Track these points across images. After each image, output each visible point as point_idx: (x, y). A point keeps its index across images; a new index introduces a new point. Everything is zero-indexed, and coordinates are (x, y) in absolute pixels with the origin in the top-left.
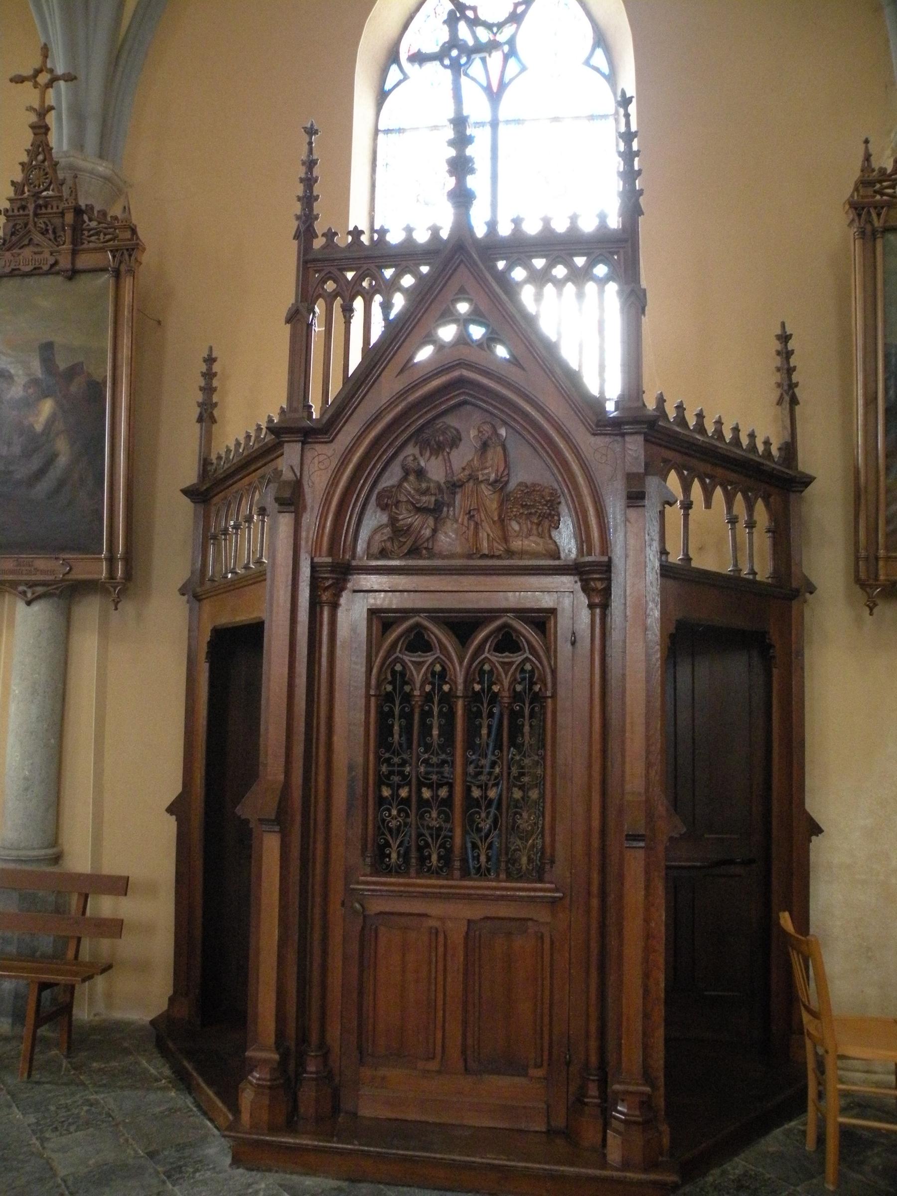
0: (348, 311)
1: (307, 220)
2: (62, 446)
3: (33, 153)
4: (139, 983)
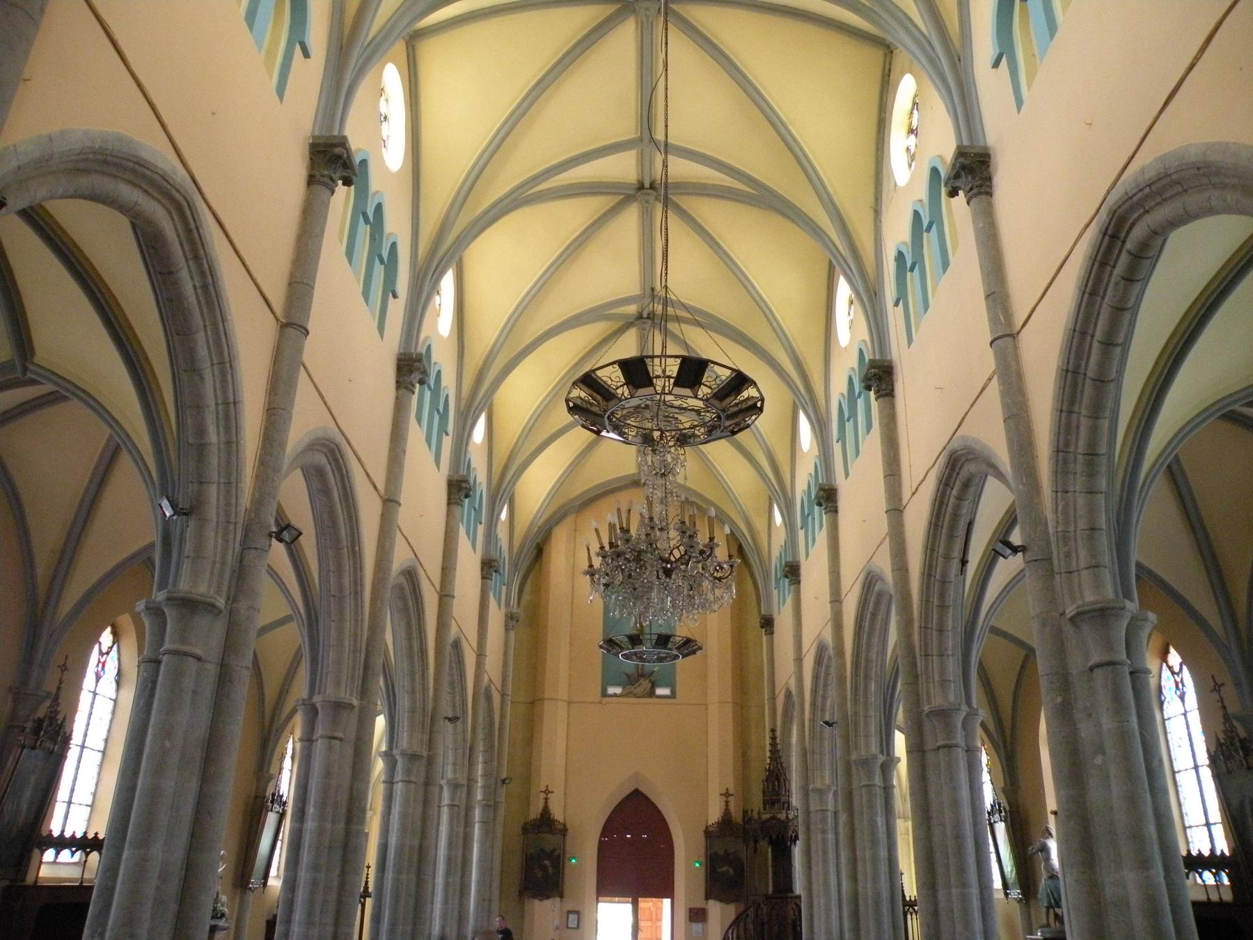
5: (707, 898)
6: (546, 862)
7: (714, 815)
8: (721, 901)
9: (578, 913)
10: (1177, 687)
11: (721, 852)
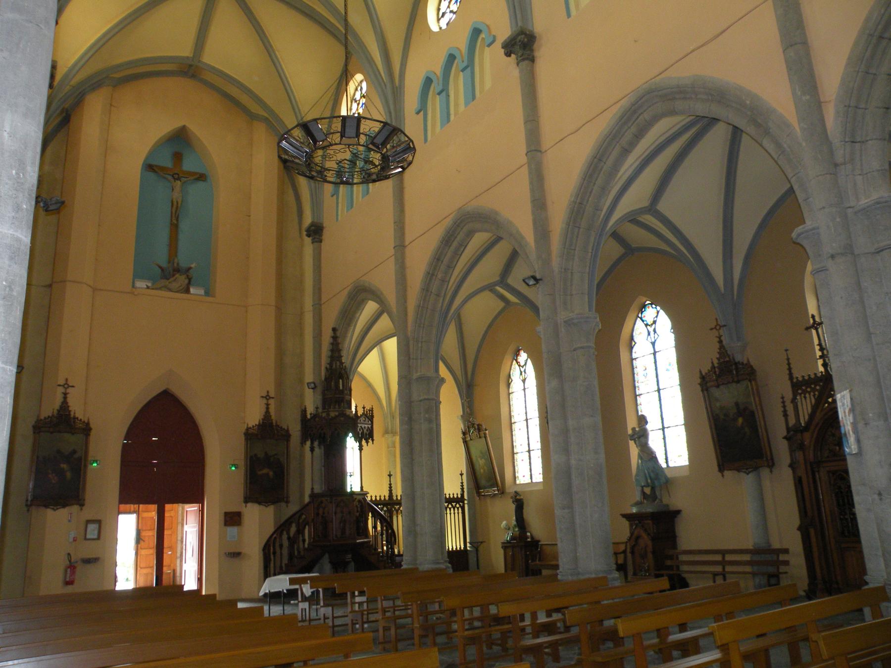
0: (805, 397)
1: (791, 375)
2: (747, 430)
3: (720, 349)
4: (797, 567)
5: (247, 500)
6: (64, 466)
7: (254, 417)
8: (259, 503)
9: (99, 522)
10: (521, 374)
11: (261, 455)
